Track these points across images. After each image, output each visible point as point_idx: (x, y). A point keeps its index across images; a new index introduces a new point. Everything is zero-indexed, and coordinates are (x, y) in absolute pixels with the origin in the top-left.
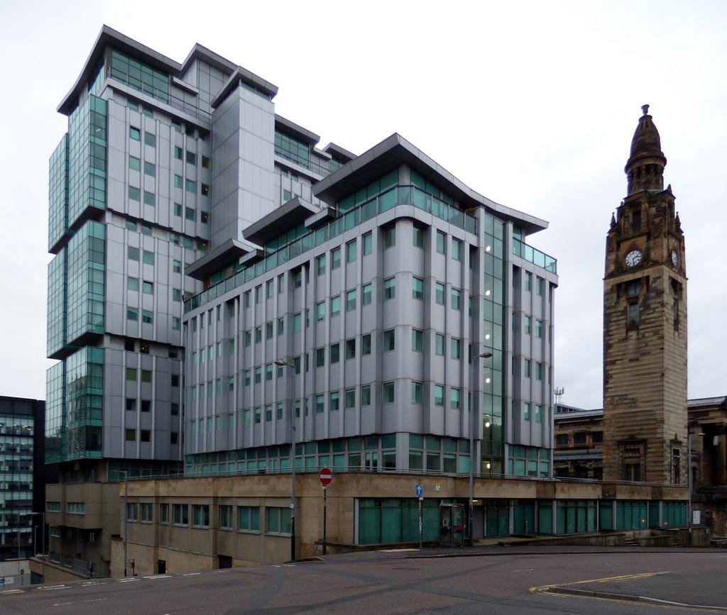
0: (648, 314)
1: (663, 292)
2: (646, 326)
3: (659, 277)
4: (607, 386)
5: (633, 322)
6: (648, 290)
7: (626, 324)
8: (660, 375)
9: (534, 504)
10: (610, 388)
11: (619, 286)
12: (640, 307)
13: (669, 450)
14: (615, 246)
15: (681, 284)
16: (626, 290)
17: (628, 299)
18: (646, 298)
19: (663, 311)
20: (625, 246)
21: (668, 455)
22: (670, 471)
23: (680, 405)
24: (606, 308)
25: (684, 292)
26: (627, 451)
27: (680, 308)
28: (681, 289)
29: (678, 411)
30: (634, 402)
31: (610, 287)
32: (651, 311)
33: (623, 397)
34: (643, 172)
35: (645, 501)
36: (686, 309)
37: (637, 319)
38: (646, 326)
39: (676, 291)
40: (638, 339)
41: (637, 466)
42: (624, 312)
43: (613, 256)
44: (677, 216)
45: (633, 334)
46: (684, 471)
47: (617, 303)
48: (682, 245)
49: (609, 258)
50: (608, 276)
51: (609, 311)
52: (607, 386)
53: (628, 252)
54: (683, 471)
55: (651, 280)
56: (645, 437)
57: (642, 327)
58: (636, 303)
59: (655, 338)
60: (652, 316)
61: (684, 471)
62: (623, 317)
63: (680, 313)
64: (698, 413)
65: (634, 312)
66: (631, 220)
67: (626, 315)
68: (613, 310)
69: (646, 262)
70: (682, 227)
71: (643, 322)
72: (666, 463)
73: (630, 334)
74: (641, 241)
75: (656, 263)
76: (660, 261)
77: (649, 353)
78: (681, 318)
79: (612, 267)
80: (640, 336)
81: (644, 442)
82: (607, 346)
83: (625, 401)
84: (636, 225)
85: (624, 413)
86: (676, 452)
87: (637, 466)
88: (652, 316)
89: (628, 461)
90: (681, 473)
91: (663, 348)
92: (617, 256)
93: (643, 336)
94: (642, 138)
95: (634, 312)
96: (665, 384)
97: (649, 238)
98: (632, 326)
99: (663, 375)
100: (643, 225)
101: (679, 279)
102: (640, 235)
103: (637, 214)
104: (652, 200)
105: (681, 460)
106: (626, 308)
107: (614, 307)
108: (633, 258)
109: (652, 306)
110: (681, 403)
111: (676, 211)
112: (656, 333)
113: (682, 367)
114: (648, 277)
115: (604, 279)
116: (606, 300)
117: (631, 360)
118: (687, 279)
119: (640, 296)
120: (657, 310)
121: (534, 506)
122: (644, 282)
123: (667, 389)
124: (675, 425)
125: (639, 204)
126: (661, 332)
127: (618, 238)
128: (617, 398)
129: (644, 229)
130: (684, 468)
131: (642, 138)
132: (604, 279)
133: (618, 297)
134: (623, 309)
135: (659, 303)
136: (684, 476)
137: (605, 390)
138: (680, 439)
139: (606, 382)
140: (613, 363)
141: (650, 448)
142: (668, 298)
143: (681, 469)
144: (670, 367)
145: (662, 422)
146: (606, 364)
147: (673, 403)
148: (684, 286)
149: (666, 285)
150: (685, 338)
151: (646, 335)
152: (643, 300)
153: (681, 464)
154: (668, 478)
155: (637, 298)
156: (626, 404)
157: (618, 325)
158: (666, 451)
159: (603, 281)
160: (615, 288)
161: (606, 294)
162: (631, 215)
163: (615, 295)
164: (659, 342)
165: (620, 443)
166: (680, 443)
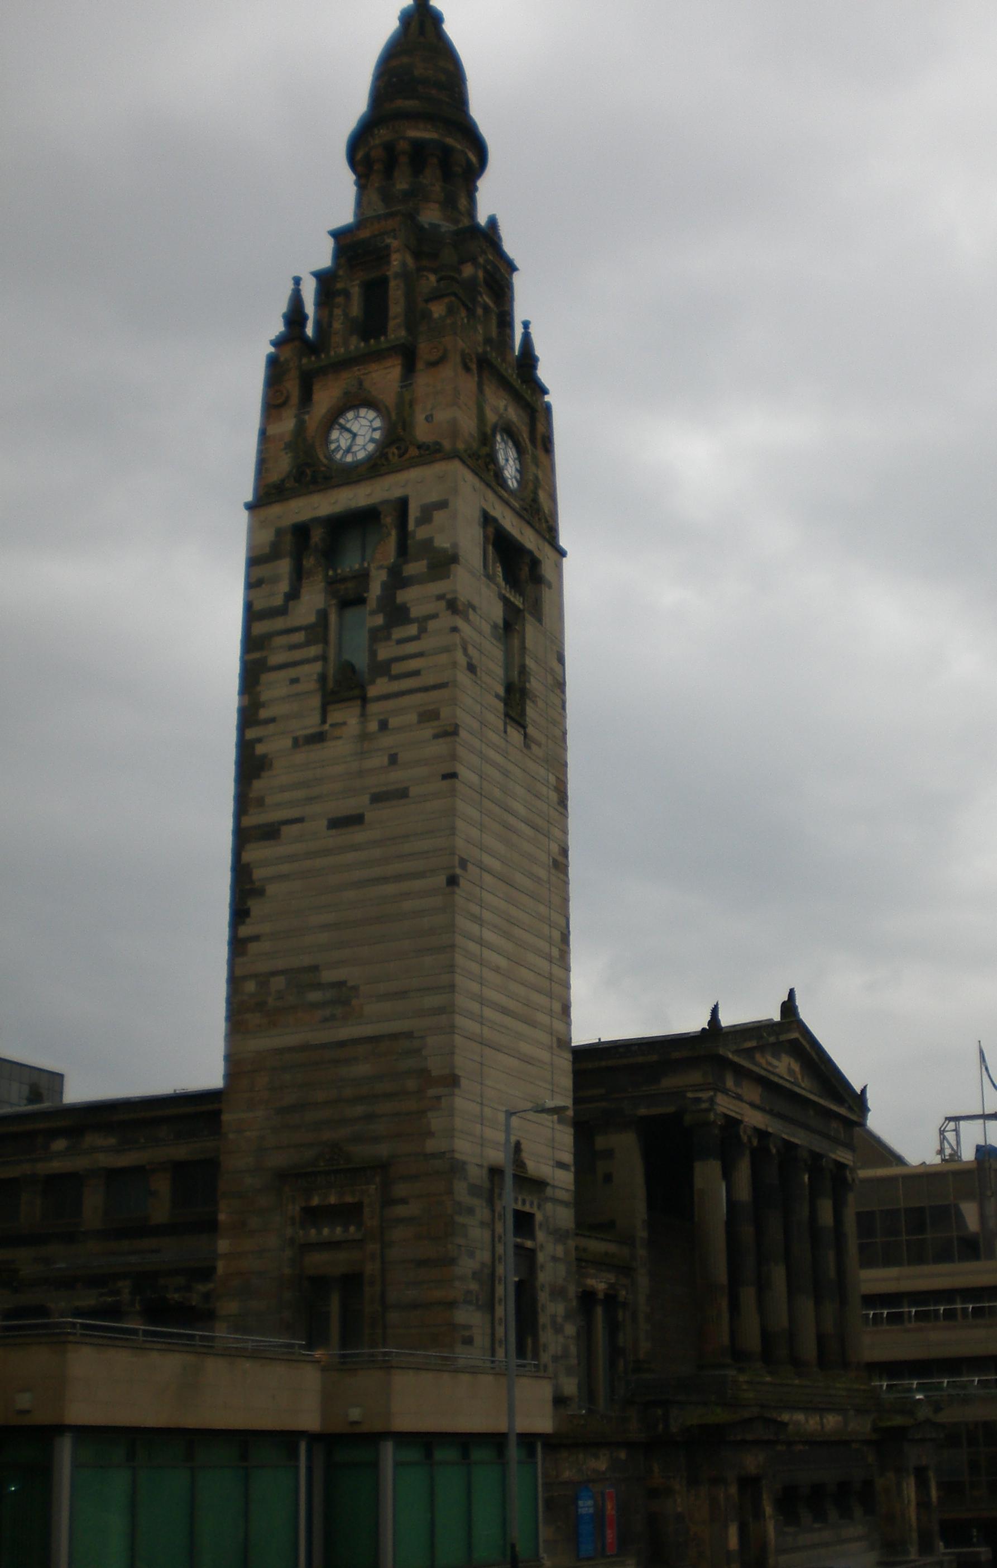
0: (399, 642)
1: (453, 559)
2: (396, 686)
3: (443, 505)
4: (244, 931)
5: (348, 669)
6: (403, 549)
7: (323, 678)
8: (441, 880)
9: (294, 1455)
10: (256, 938)
11: (301, 531)
12: (373, 613)
13: (482, 1212)
14: (292, 386)
15: (535, 563)
16: (331, 554)
17: (332, 584)
18: (397, 580)
19: (455, 629)
20: (326, 396)
21: (478, 1234)
22: (490, 1306)
23: (533, 1024)
24: (252, 615)
25: (547, 594)
26: (313, 1215)
27: (529, 644)
28: (537, 578)
29: (526, 1048)
30: (343, 997)
31: (267, 536)
32: (413, 630)
33: (304, 978)
34: (404, 160)
35: (286, 1440)
36: (561, 659)
37: (361, 661)
38: (396, 686)
39: (512, 579)
40: (364, 736)
41: (351, 1282)
42: (318, 631)
43: (287, 425)
44: (527, 337)
45: (347, 716)
46: (558, 1309)
47: (293, 595)
48: (541, 428)
49: (272, 430)
50: (267, 496)
51: (260, 628)
52: (244, 931)
53: (333, 419)
54: (552, 1309)
55: (414, 512)
56: (383, 1150)
57: (379, 687)
58: (361, 601)
59: (427, 732)
60: (411, 648)
61: (558, 1309)
62: (313, 651)
63: (529, 662)
64: (604, 1067)
65: (355, 637)
66: (356, 309)
67: (325, 641)
68: (279, 623)
69: (398, 448)
70: (544, 373)
71: (382, 669)
72: (467, 1265)
73: (336, 715)
74: (385, 378)
75: (431, 453)
76: (447, 444)
77: (402, 794)
78: (534, 685)
79: (283, 465)
80: (373, 726)
81: (382, 1167)
82: (250, 765)
83: (315, 996)
84: (372, 323)
85: (305, 1048)
86: (524, 1222)
87: (351, 1282)
88: (411, 648)
89: (318, 1261)
90: (543, 1319)
91: (453, 776)
92: (301, 427)
93: (384, 725)
94: (405, 60)
95: (355, 637)
96: (463, 923)
97: (409, 369)
98: (345, 687)
99: (453, 881)
100: (392, 324)
101: (529, 539)
102: (377, 356)
103: (375, 292)
104: (425, 245)
105: (541, 1257)
106: (323, 615)
107: (281, 611)
108: (360, 434)
109: (415, 612)
110: (543, 1018)
111: (521, 312)
112: (429, 716)
113: (543, 874)
114: (402, 505)
115: (250, 507)
116: (252, 584)
117: (338, 823)
118: (562, 553)
119: (373, 573)
120: (432, 625)
121: (297, 1468)
122: (388, 519)
123: (473, 947)
124: (505, 1116)
125: (382, 256)
126: (445, 712)
127: (302, 368)
128: (278, 983)
129: (396, 332)
130: (558, 1293)
131: (405, 60)
132: (250, 507)
133: (298, 575)
134: (312, 619)
135: (440, 597)
136: (558, 1330)
137: (238, 945)
138: (537, 1166)
139: (239, 914)
140: (270, 833)
141: (403, 1201)
142: (476, 584)
143: (543, 1297)
144: (488, 860)
145: (453, 1081)
146: (242, 837)
147: (505, 1011)
148: (547, 570)
149: (469, 542)
150: (558, 765)
151: (393, 722)
152: (385, 586)
153: (543, 1277)
154: (481, 1340)
155: (363, 577)
156: (315, 1006)
157: (295, 681)
158: (471, 1211)
159: (245, 515)
160: (288, 540)
161: (253, 562)
162: (356, 291)
163: (284, 566)
164: (440, 748)
165: (284, 1177)
166: (538, 1185)
